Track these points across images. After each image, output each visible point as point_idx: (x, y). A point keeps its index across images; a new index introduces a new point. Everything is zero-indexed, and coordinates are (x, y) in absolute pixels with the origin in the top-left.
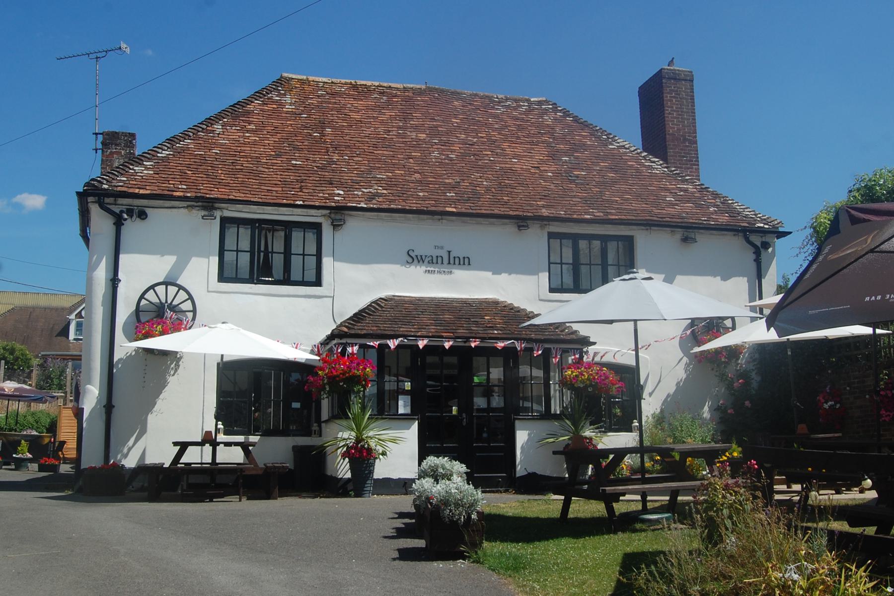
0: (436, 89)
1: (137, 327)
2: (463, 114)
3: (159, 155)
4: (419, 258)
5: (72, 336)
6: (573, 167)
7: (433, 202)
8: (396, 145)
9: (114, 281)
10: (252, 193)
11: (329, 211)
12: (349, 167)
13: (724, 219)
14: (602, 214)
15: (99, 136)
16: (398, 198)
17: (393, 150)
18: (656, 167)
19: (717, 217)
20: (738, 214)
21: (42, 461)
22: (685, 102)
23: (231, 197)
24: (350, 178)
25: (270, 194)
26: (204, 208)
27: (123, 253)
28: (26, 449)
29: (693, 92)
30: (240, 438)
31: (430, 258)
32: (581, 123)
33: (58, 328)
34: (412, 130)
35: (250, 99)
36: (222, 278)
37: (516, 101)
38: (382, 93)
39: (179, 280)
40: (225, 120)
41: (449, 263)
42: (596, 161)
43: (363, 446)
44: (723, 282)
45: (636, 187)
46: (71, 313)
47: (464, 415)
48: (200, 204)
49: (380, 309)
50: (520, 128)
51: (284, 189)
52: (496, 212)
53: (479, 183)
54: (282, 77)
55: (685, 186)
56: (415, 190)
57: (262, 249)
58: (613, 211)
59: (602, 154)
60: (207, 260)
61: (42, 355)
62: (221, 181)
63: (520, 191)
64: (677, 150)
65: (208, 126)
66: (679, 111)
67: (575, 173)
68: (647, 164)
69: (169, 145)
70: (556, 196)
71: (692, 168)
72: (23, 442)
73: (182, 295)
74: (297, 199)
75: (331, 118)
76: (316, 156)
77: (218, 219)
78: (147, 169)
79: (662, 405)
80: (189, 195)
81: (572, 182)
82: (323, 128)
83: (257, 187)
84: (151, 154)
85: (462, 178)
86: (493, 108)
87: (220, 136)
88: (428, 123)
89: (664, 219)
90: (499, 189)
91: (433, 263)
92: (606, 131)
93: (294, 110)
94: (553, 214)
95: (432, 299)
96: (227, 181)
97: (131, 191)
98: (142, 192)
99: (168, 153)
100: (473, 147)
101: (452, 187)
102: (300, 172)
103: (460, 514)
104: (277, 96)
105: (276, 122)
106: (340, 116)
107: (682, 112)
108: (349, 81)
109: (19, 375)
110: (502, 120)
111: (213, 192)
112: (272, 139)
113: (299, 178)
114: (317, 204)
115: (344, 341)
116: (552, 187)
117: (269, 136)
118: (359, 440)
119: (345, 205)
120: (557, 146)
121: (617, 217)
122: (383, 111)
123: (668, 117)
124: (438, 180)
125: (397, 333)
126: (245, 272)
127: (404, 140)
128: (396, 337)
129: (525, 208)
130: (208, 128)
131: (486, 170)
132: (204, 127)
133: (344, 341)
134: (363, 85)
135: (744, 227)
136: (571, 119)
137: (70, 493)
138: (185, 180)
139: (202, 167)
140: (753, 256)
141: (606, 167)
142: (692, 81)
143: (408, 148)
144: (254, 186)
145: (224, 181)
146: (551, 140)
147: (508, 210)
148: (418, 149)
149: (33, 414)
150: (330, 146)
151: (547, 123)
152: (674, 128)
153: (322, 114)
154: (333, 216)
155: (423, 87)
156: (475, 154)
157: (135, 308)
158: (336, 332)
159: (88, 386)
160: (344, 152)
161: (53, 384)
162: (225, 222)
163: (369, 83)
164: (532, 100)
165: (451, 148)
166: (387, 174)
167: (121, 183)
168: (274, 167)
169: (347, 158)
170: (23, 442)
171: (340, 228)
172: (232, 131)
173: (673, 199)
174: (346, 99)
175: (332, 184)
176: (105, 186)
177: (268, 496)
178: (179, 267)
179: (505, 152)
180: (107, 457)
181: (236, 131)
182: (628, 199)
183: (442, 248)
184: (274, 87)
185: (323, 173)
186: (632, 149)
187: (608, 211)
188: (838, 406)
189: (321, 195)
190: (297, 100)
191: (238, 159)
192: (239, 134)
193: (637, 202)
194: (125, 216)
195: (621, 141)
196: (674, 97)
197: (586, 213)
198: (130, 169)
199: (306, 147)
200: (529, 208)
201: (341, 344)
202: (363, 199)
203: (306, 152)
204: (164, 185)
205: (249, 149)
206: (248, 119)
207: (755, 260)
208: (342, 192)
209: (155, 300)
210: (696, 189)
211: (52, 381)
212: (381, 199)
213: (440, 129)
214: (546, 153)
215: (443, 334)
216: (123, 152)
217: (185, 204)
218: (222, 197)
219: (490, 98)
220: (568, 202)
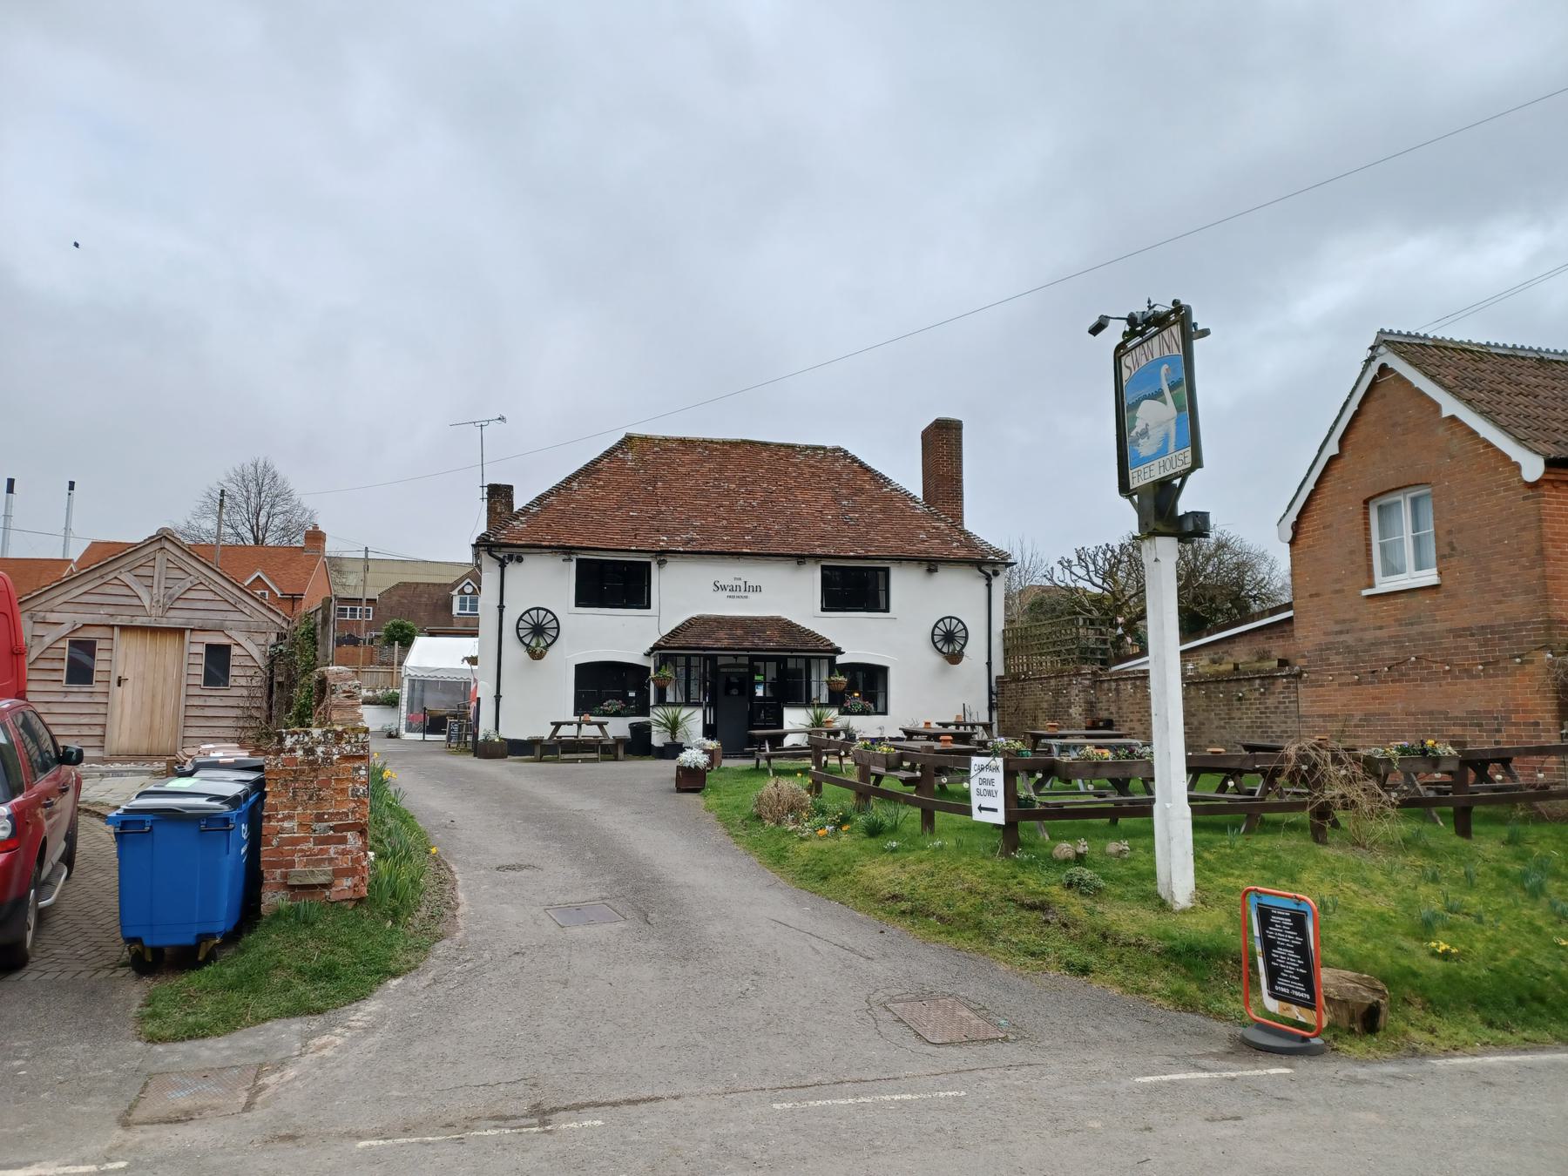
2: (770, 464)
13: (962, 553)
23: (584, 545)
52: (781, 551)
77: (575, 560)
78: (522, 523)
84: (525, 511)
97: (511, 542)
98: (519, 542)
101: (749, 532)
110: (799, 468)
140: (986, 582)
176: (493, 539)
182: (887, 538)
196: (945, 444)
197: (851, 551)
208: (665, 538)
212: (694, 543)
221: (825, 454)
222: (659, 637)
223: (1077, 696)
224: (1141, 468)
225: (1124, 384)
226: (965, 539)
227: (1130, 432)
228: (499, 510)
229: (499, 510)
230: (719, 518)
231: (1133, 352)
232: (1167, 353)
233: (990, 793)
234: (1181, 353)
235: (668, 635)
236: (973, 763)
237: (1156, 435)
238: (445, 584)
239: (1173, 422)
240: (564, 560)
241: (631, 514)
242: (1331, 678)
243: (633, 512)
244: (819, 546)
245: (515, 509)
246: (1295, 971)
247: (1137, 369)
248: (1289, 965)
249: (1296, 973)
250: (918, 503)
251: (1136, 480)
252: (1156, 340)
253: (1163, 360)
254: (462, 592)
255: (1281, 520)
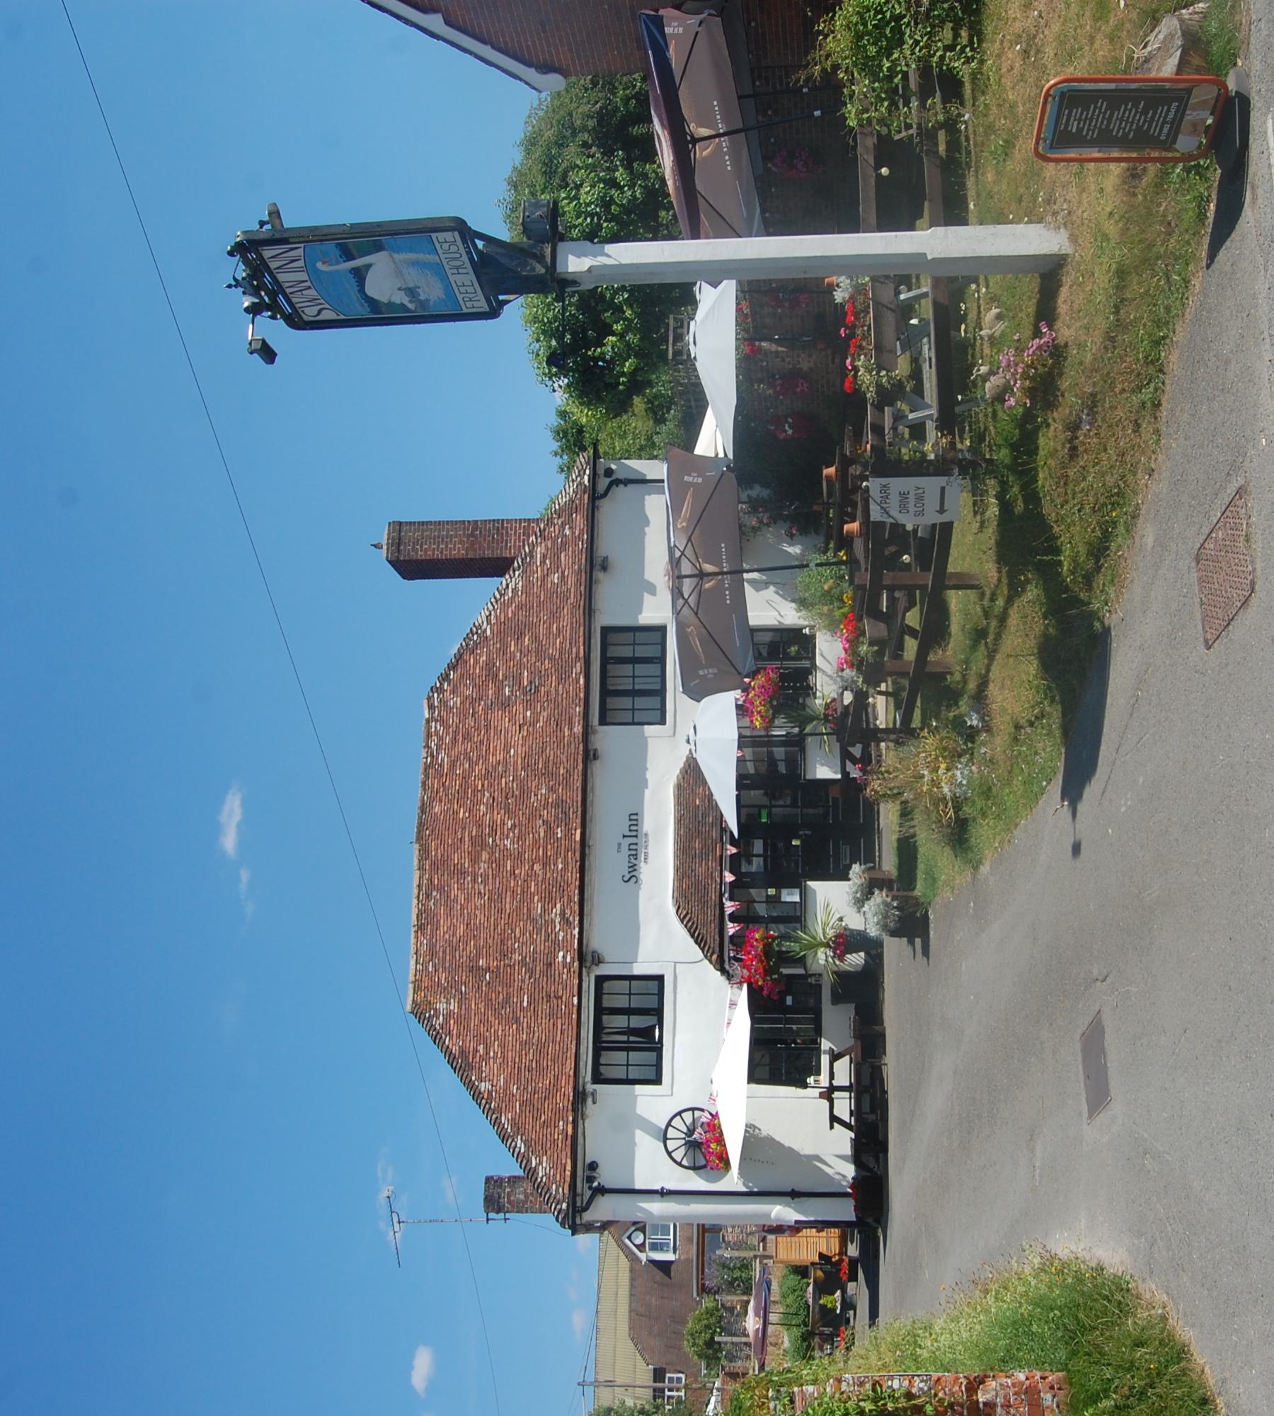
0: (419, 832)
1: (712, 1168)
2: (451, 802)
3: (522, 1150)
4: (631, 869)
5: (669, 1256)
6: (518, 684)
7: (570, 853)
8: (497, 886)
9: (664, 1193)
10: (565, 1051)
11: (584, 969)
12: (529, 942)
13: (580, 520)
14: (578, 664)
15: (490, 1217)
16: (565, 892)
17: (504, 892)
18: (513, 583)
19: (578, 528)
20: (573, 502)
21: (845, 1278)
22: (428, 533)
23: (572, 1073)
24: (543, 942)
25: (566, 1032)
26: (584, 1101)
27: (634, 1185)
28: (830, 1298)
29: (415, 522)
30: (825, 1060)
31: (631, 857)
32: (457, 661)
33: (659, 1275)
34: (476, 866)
35: (444, 1050)
36: (657, 1080)
37: (429, 735)
38: (428, 896)
39: (659, 1125)
40: (473, 1078)
41: (636, 836)
42: (508, 655)
43: (834, 942)
44: (651, 525)
45: (542, 615)
46: (638, 1260)
47: (801, 833)
48: (580, 1106)
49: (689, 916)
50: (467, 737)
51: (559, 1016)
52: (579, 784)
53: (543, 798)
54: (412, 1012)
55: (539, 556)
56: (555, 871)
57: (624, 1038)
58: (574, 650)
59: (498, 646)
60: (639, 1098)
61: (698, 1295)
62: (552, 1084)
63: (552, 753)
64: (486, 545)
65: (483, 1098)
66: (439, 542)
67: (526, 684)
68: (510, 594)
69: (510, 1140)
70: (556, 712)
71: (507, 527)
72: (821, 1302)
73: (677, 1122)
74: (571, 1003)
75: (465, 958)
76: (516, 979)
77: (595, 1086)
78: (541, 1163)
79: (786, 599)
80: (571, 1119)
81: (537, 690)
82: (479, 968)
83: (557, 1046)
84: (523, 1159)
85: (538, 817)
86: (441, 765)
87: (495, 1084)
88: (466, 847)
89: (583, 593)
90: (550, 776)
91: (636, 855)
92: (468, 634)
93: (457, 1000)
94: (579, 721)
95: (676, 857)
96: (552, 1078)
97: (568, 1179)
98: (569, 1167)
99: (519, 1141)
100: (496, 797)
101: (550, 830)
102: (537, 998)
103: (894, 915)
104: (438, 1018)
105: (473, 1021)
106: (461, 948)
107: (439, 537)
108: (413, 935)
109: (729, 1322)
110: (458, 758)
111: (567, 1093)
112: (496, 1026)
113: (545, 999)
114: (576, 981)
115: (727, 959)
116: (545, 714)
117: (492, 1030)
118: (827, 945)
119: (576, 952)
120: (490, 697)
121: (582, 648)
122: (453, 897)
123: (446, 555)
124: (541, 845)
125: (718, 902)
126: (650, 1057)
127: (490, 877)
128: (722, 906)
129: (573, 751)
130: (486, 1097)
131: (526, 788)
132: (484, 1101)
133: (727, 959)
134: (417, 917)
135: (589, 498)
136: (452, 673)
137: (880, 1230)
138: (553, 1122)
139: (536, 1104)
140: (621, 486)
141: (516, 645)
142: (400, 523)
143: (501, 874)
144: (557, 1048)
145: (552, 1081)
146: (483, 703)
147: (576, 771)
148: (502, 862)
149: (784, 1296)
150: (502, 963)
151: (459, 703)
152: (459, 548)
153: (460, 969)
154: (588, 964)
155: (417, 846)
156: (506, 797)
157: (691, 1171)
158: (718, 967)
159: (773, 1215)
160: (510, 947)
161: (741, 1277)
162: (598, 1079)
163: (415, 911)
164: (427, 716)
165: (499, 823)
166: (536, 901)
167: (559, 1190)
168: (533, 1025)
169: (517, 945)
170: (821, 1302)
171: (601, 957)
172: (487, 1071)
173: (556, 575)
174: (438, 938)
175: (551, 964)
176: (564, 1206)
177: (882, 1036)
178: (647, 1126)
179: (501, 762)
180: (845, 1195)
181: (488, 1067)
182: (558, 628)
183: (619, 844)
184: (426, 1022)
185: (538, 972)
186: (491, 608)
187: (574, 656)
188: (790, 420)
189: (565, 976)
190: (442, 995)
191: (523, 1065)
192: (491, 1063)
193: (562, 619)
194: (595, 1184)
195: (481, 619)
196: (421, 547)
197: (578, 682)
198: (542, 1181)
199: (505, 989)
200: (573, 746)
201: (729, 961)
202: (569, 931)
203: (511, 989)
204: (560, 1145)
205: (510, 1053)
206: (471, 1053)
207: (626, 486)
208: (561, 954)
209: (682, 1150)
210: (541, 543)
211: (736, 1279)
212: (568, 911)
213: (474, 834)
214: (500, 712)
215: (718, 854)
216: (507, 1190)
217: (580, 1122)
218: (571, 1083)
219: (427, 768)
220: (564, 700)
221: (436, 721)
222: (707, 962)
223: (783, 360)
224: (460, 298)
225: (342, 317)
226: (559, 517)
227: (409, 311)
228: (522, 1197)
229: (522, 1197)
230: (531, 874)
231: (297, 306)
232: (301, 263)
233: (919, 498)
234: (302, 245)
235: (703, 950)
236: (879, 519)
237: (413, 277)
238: (631, 1271)
239: (396, 256)
240: (594, 1103)
241: (525, 1004)
242: (753, 24)
243: (522, 1002)
244: (571, 729)
245: (520, 1173)
246: (1141, 113)
247: (322, 301)
248: (1134, 119)
249: (1145, 112)
250: (508, 585)
251: (476, 304)
252: (281, 277)
253: (309, 268)
254: (641, 1247)
255: (534, 88)
